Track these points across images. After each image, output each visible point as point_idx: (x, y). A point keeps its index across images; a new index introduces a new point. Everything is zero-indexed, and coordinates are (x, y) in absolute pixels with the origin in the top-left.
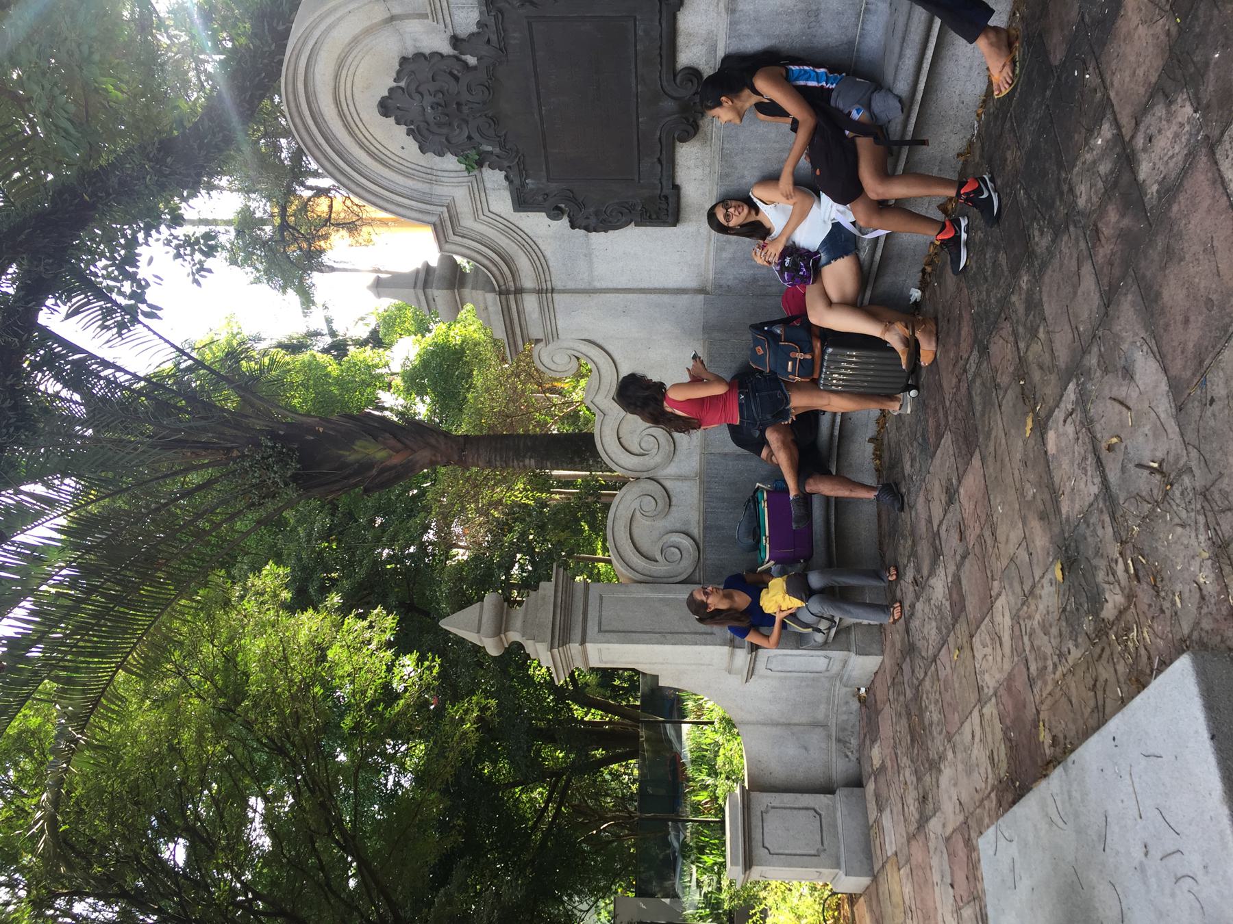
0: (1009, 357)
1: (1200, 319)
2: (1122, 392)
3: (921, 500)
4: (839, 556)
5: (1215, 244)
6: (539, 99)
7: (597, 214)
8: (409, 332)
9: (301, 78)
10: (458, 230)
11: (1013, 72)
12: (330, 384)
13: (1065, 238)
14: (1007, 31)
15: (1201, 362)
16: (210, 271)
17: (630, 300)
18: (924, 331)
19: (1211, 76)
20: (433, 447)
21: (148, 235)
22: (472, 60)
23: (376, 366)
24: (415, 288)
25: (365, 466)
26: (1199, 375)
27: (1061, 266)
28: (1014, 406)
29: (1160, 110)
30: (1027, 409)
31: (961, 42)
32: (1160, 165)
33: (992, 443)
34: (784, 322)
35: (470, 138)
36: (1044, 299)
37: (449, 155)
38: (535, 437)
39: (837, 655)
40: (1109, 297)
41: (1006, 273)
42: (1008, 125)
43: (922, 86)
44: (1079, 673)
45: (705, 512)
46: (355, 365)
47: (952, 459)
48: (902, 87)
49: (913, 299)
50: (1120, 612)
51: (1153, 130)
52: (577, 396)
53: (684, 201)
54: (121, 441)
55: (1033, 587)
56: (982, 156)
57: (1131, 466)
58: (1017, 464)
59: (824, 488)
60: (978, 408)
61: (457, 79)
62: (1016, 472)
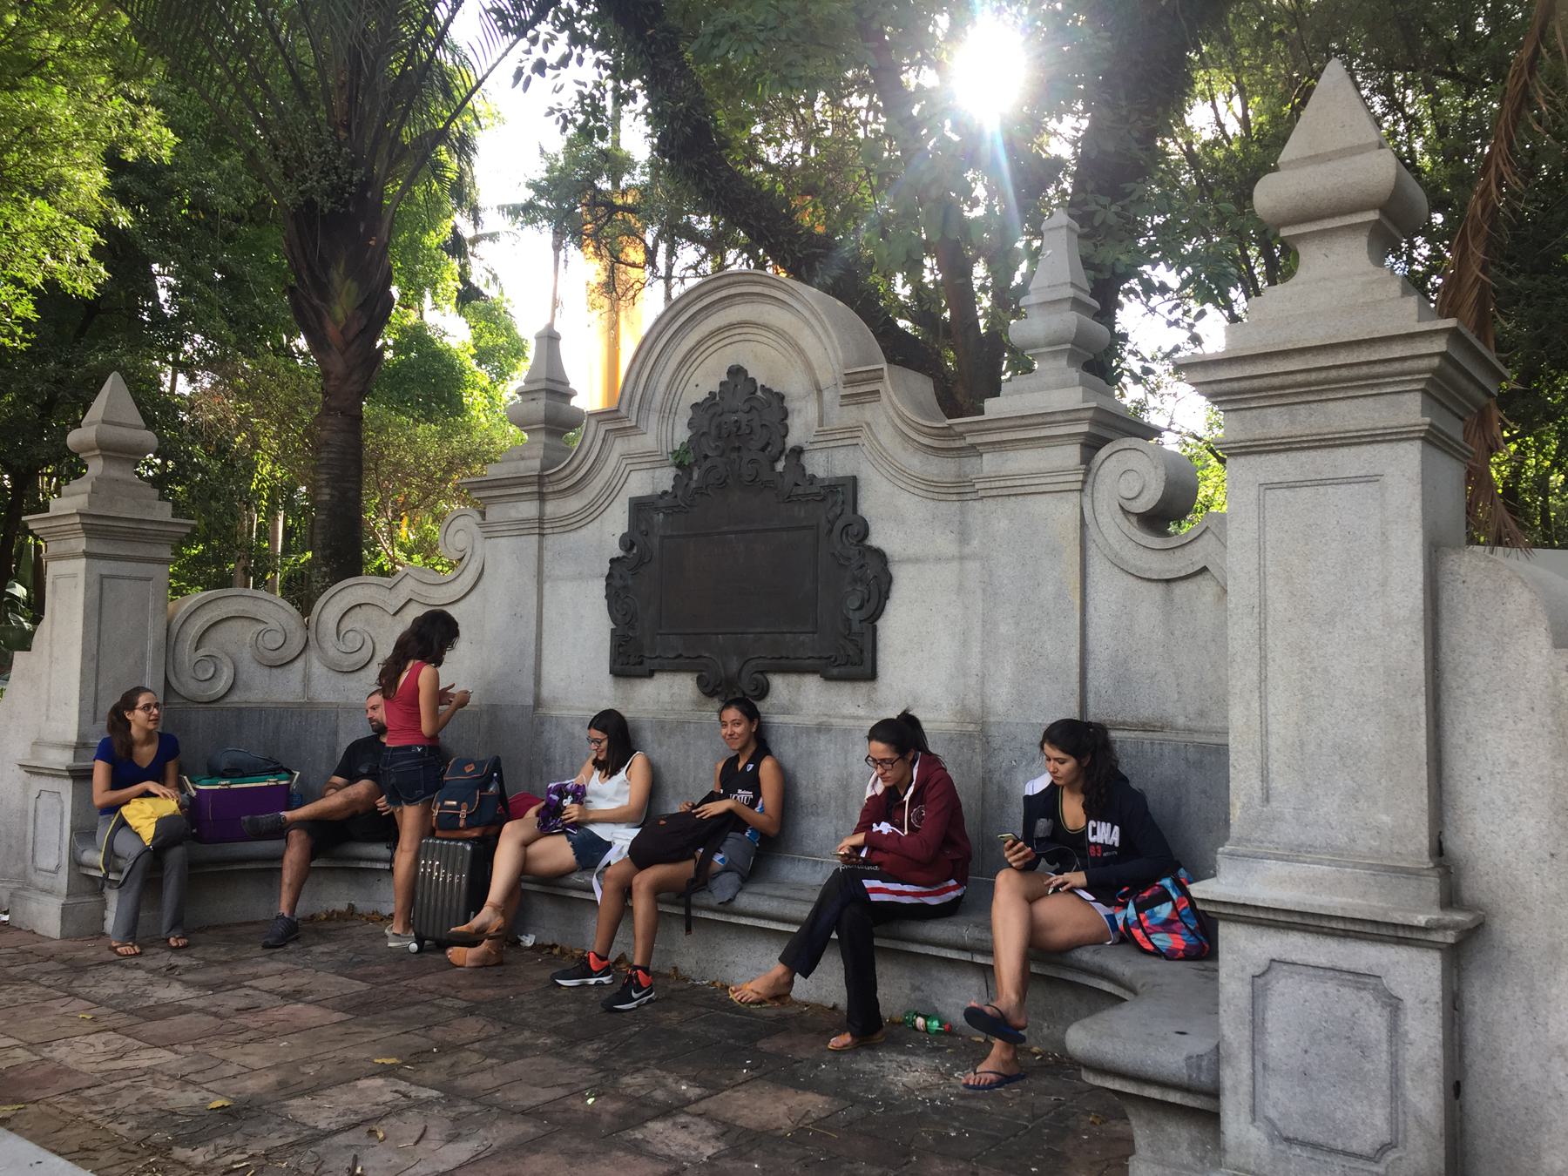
2: (433, 1134)
3: (282, 966)
4: (199, 877)
6: (743, 532)
10: (611, 436)
17: (537, 624)
22: (780, 466)
25: (323, 290)
30: (406, 1058)
32: (660, 1137)
35: (706, 457)
37: (689, 434)
39: (62, 880)
40: (527, 1113)
42: (703, 1010)
43: (743, 921)
44: (98, 1135)
45: (261, 709)
46: (438, 266)
48: (744, 901)
49: (523, 938)
50: (183, 1163)
51: (693, 1128)
53: (637, 682)
55: (194, 1083)
58: (340, 1055)
59: (293, 853)
60: (401, 1013)
61: (763, 449)
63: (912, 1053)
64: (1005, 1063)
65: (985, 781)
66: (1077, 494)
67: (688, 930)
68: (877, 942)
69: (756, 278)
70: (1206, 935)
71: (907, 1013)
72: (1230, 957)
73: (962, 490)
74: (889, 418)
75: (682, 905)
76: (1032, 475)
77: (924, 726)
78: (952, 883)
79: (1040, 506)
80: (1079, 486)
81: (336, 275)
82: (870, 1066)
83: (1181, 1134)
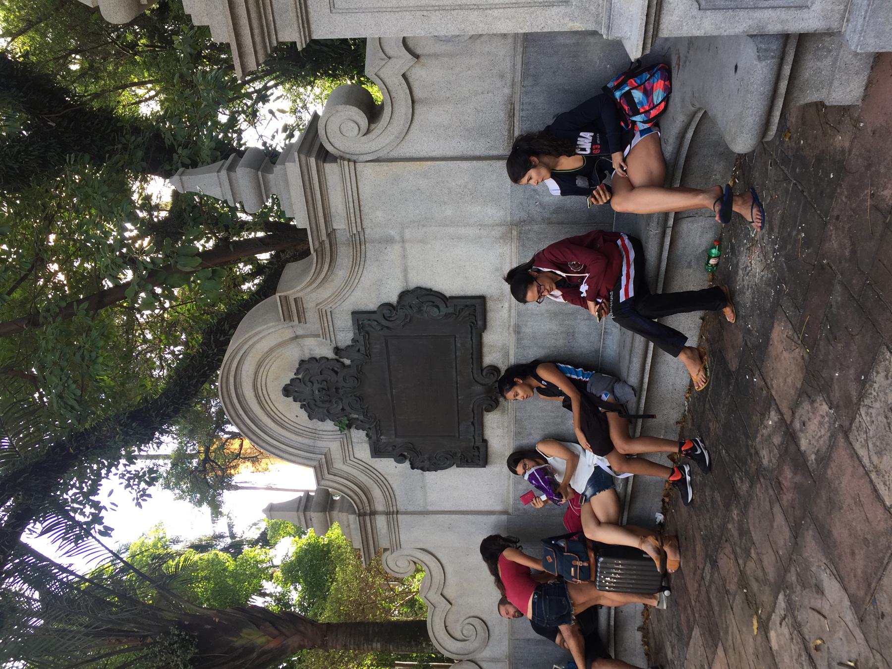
0: (733, 570)
1: (862, 552)
2: (818, 604)
5: (862, 499)
7: (429, 459)
8: (290, 534)
9: (232, 373)
10: (333, 470)
11: (706, 375)
12: (226, 577)
13: (759, 486)
14: (698, 349)
15: (869, 585)
16: (149, 496)
18: (671, 546)
19: (836, 387)
20: (301, 632)
21: (109, 471)
22: (347, 362)
23: (262, 562)
24: (298, 511)
26: (869, 595)
27: (759, 504)
28: (742, 609)
29: (806, 406)
31: (669, 357)
33: (730, 637)
34: (567, 537)
35: (343, 409)
36: (751, 528)
37: (328, 421)
38: (381, 625)
40: (796, 532)
41: (722, 507)
42: (707, 406)
43: (646, 380)
46: (247, 561)
47: (702, 648)
48: (633, 380)
49: (658, 521)
51: (804, 418)
52: (416, 585)
53: (490, 450)
54: (64, 630)
56: (693, 425)
57: (834, 664)
58: (751, 657)
60: (716, 608)
61: (336, 373)
62: (751, 663)
63: (737, 266)
64: (745, 202)
65: (550, 222)
66: (357, 165)
67: (653, 417)
68: (660, 292)
69: (224, 381)
70: (652, 67)
71: (707, 270)
72: (685, 28)
73: (358, 242)
74: (312, 291)
75: (636, 422)
76: (345, 195)
77: (515, 265)
78: (619, 242)
79: (366, 189)
80: (352, 164)
81: (238, 642)
82: (748, 294)
83: (812, 66)
